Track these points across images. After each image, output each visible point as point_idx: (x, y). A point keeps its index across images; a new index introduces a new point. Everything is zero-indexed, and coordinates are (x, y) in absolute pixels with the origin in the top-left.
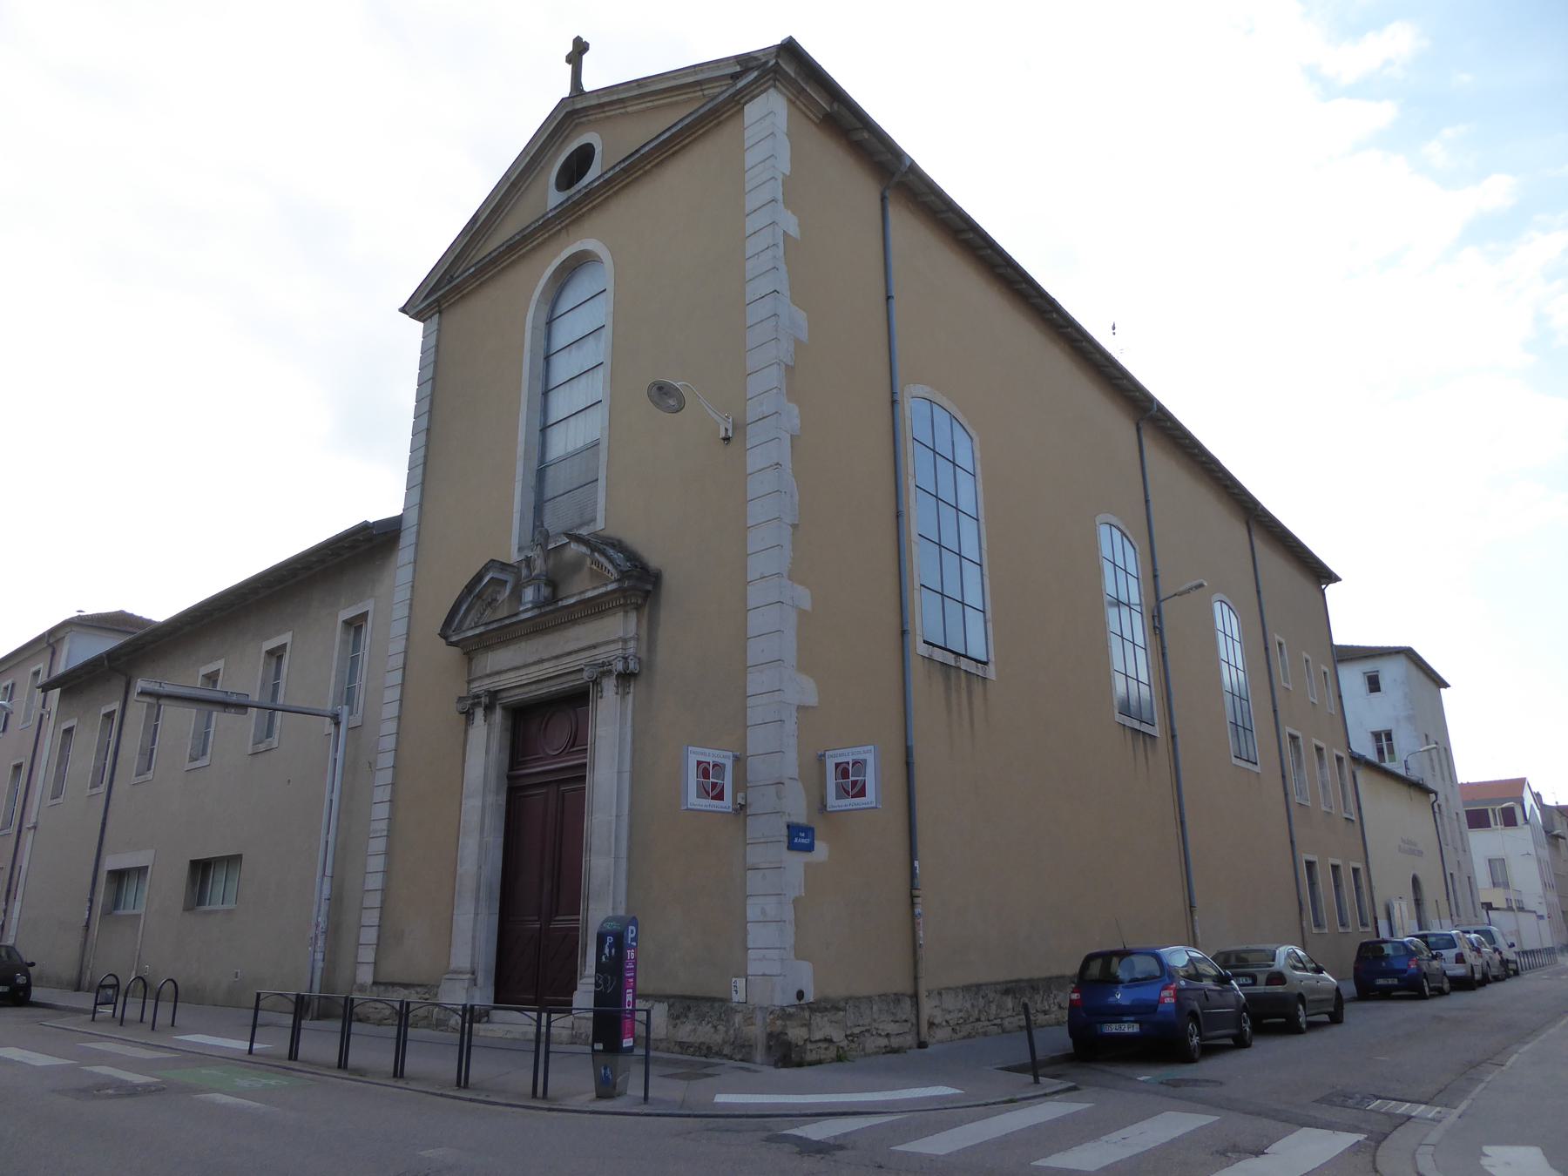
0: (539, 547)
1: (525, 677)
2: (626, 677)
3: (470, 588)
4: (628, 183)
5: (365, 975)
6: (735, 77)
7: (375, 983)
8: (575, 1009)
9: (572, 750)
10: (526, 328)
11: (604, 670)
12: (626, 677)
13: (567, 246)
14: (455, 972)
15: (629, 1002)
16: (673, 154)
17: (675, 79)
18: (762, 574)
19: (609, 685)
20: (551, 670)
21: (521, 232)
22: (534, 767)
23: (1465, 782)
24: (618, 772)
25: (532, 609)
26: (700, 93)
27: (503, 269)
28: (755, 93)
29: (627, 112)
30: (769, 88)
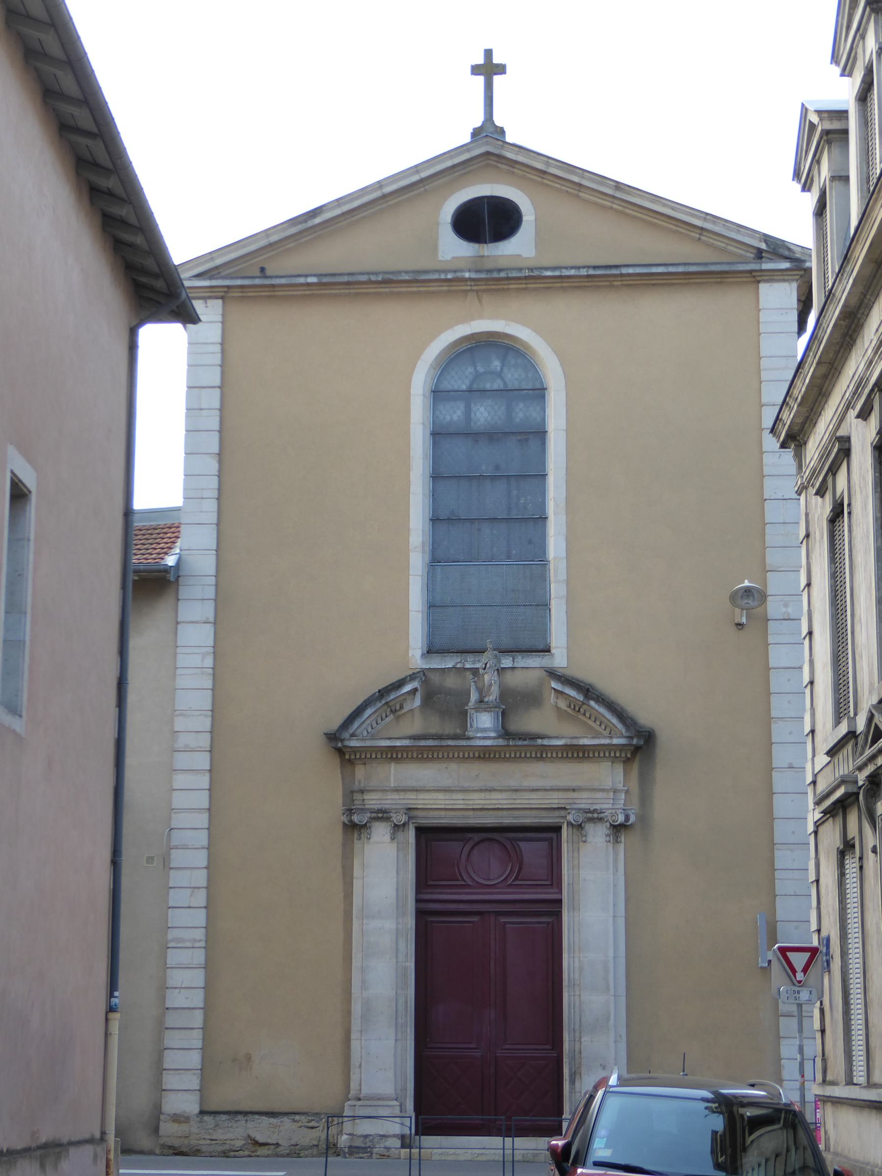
0: (496, 672)
1: (462, 802)
2: (618, 829)
3: (383, 693)
4: (585, 287)
5: (190, 1105)
6: (759, 254)
7: (202, 1112)
8: (420, 1138)
9: (515, 883)
10: (413, 391)
11: (594, 817)
12: (618, 829)
13: (481, 317)
14: (369, 1098)
15: (818, 1118)
16: (654, 285)
17: (673, 209)
18: (791, 764)
19: (597, 835)
20: (505, 802)
21: (413, 272)
22: (431, 893)
23: (172, 857)
24: (614, 917)
25: (494, 738)
26: (698, 236)
27: (357, 294)
28: (776, 278)
29: (578, 196)
30: (793, 280)
